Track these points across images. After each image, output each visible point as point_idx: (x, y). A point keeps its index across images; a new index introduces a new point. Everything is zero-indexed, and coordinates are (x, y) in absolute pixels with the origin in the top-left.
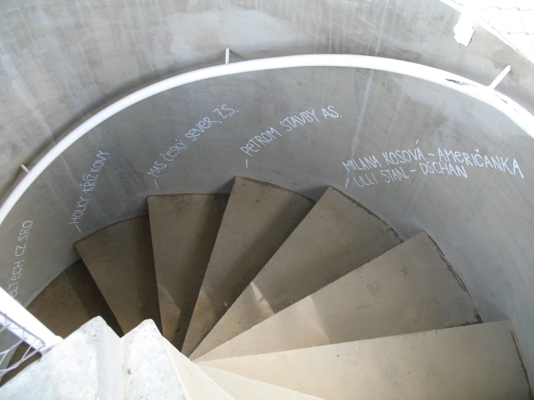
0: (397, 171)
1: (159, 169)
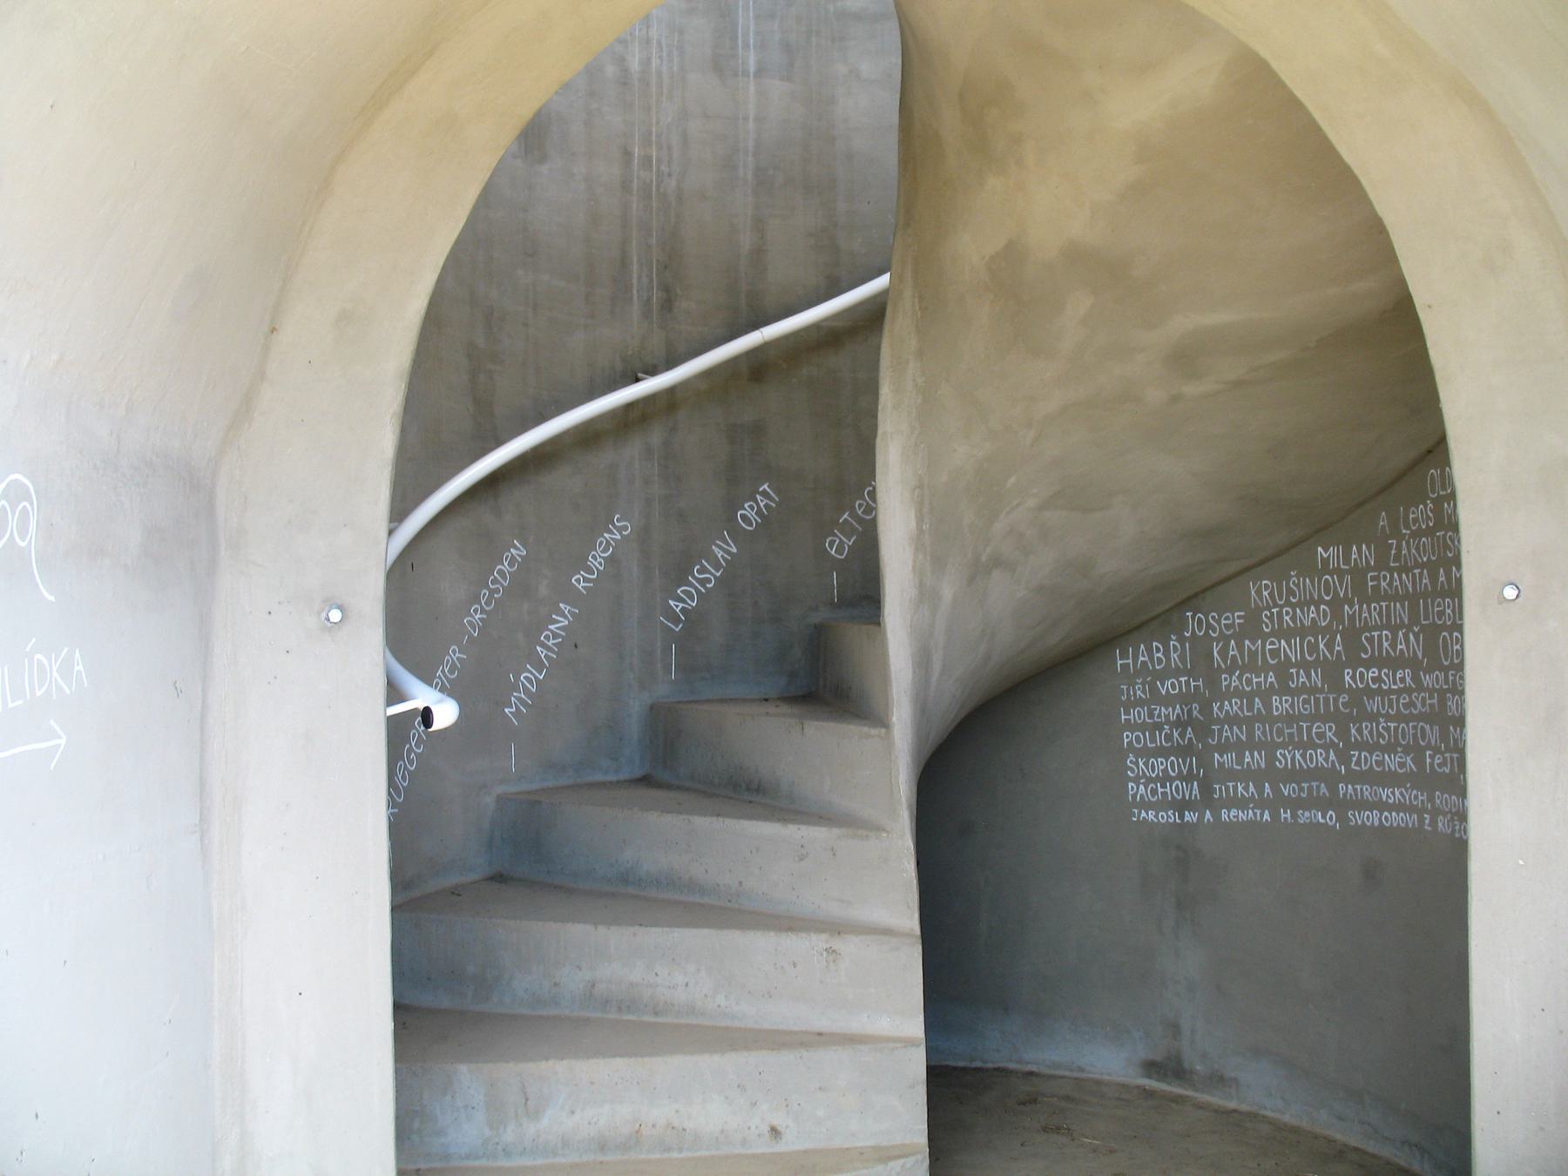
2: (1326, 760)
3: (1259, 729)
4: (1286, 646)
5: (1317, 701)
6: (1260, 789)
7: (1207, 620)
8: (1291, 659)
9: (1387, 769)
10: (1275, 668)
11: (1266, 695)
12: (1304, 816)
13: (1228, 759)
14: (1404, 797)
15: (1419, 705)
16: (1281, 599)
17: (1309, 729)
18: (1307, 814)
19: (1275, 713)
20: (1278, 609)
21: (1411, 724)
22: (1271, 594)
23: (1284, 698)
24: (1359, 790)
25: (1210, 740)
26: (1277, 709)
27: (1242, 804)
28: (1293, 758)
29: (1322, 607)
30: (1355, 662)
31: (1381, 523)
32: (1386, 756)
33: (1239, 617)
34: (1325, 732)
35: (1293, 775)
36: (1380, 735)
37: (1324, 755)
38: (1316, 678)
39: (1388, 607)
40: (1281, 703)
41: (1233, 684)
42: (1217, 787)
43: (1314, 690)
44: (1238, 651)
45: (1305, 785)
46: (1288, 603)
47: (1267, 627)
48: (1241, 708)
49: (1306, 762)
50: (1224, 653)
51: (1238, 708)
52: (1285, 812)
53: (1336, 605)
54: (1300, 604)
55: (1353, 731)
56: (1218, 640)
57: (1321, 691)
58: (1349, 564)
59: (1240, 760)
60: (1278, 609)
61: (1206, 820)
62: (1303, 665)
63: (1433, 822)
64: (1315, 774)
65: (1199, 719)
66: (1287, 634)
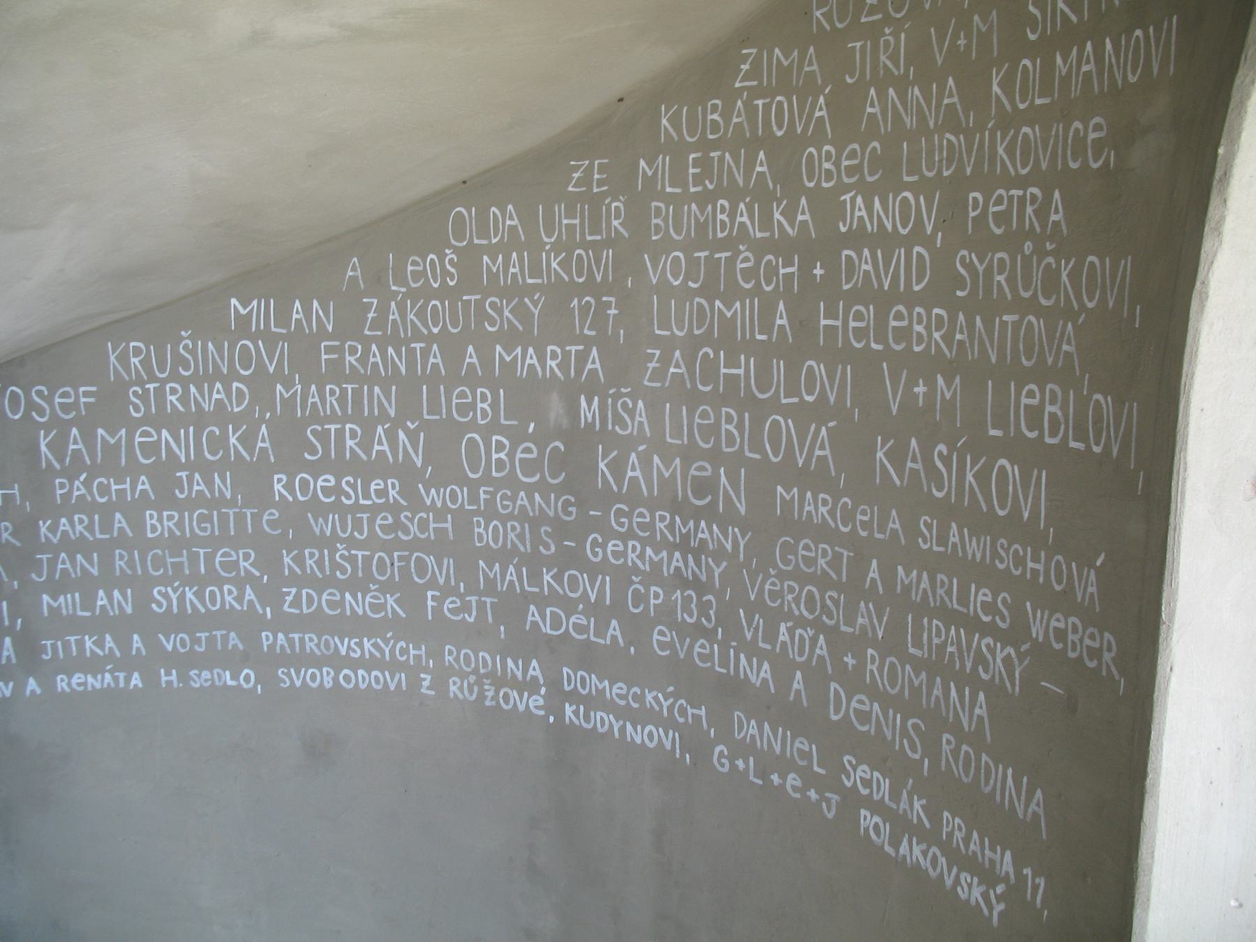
0: (953, 693)
1: (937, 697)
2: (240, 599)
3: (121, 558)
4: (170, 439)
5: (223, 519)
6: (124, 644)
7: (823, 599)
8: (178, 458)
9: (348, 613)
10: (150, 471)
11: (134, 510)
12: (201, 678)
13: (68, 603)
14: (382, 652)
15: (414, 529)
16: (162, 370)
17: (210, 559)
18: (206, 674)
19: (150, 535)
20: (157, 385)
21: (396, 554)
22: (146, 363)
23: (165, 513)
24: (297, 640)
25: (34, 576)
26: (154, 529)
27: (94, 665)
28: (182, 598)
29: (235, 385)
30: (292, 464)
31: (350, 273)
32: (348, 596)
33: (86, 394)
34: (237, 562)
35: (181, 621)
36: (335, 566)
37: (235, 593)
38: (223, 485)
39: (357, 394)
40: (160, 520)
41: (76, 493)
42: (49, 643)
43: (218, 502)
44: (84, 443)
45: (203, 635)
46: (174, 376)
47: (137, 409)
48: (90, 528)
49: (203, 603)
50: (58, 447)
51: (85, 528)
52: (168, 673)
53: (261, 384)
54: (197, 380)
55: (287, 560)
56: (47, 427)
57: (232, 503)
58: (288, 326)
59: (88, 603)
60: (157, 385)
61: (28, 692)
62: (198, 465)
63: (440, 684)
64: (224, 618)
65: (14, 546)
66: (173, 422)
